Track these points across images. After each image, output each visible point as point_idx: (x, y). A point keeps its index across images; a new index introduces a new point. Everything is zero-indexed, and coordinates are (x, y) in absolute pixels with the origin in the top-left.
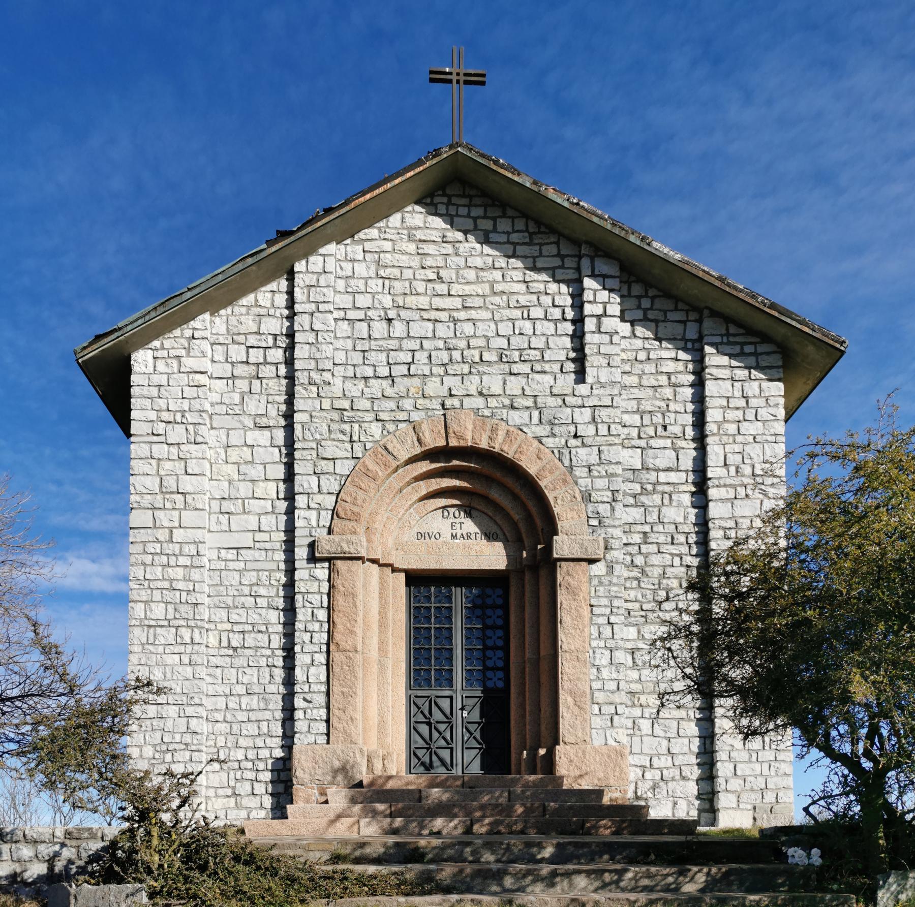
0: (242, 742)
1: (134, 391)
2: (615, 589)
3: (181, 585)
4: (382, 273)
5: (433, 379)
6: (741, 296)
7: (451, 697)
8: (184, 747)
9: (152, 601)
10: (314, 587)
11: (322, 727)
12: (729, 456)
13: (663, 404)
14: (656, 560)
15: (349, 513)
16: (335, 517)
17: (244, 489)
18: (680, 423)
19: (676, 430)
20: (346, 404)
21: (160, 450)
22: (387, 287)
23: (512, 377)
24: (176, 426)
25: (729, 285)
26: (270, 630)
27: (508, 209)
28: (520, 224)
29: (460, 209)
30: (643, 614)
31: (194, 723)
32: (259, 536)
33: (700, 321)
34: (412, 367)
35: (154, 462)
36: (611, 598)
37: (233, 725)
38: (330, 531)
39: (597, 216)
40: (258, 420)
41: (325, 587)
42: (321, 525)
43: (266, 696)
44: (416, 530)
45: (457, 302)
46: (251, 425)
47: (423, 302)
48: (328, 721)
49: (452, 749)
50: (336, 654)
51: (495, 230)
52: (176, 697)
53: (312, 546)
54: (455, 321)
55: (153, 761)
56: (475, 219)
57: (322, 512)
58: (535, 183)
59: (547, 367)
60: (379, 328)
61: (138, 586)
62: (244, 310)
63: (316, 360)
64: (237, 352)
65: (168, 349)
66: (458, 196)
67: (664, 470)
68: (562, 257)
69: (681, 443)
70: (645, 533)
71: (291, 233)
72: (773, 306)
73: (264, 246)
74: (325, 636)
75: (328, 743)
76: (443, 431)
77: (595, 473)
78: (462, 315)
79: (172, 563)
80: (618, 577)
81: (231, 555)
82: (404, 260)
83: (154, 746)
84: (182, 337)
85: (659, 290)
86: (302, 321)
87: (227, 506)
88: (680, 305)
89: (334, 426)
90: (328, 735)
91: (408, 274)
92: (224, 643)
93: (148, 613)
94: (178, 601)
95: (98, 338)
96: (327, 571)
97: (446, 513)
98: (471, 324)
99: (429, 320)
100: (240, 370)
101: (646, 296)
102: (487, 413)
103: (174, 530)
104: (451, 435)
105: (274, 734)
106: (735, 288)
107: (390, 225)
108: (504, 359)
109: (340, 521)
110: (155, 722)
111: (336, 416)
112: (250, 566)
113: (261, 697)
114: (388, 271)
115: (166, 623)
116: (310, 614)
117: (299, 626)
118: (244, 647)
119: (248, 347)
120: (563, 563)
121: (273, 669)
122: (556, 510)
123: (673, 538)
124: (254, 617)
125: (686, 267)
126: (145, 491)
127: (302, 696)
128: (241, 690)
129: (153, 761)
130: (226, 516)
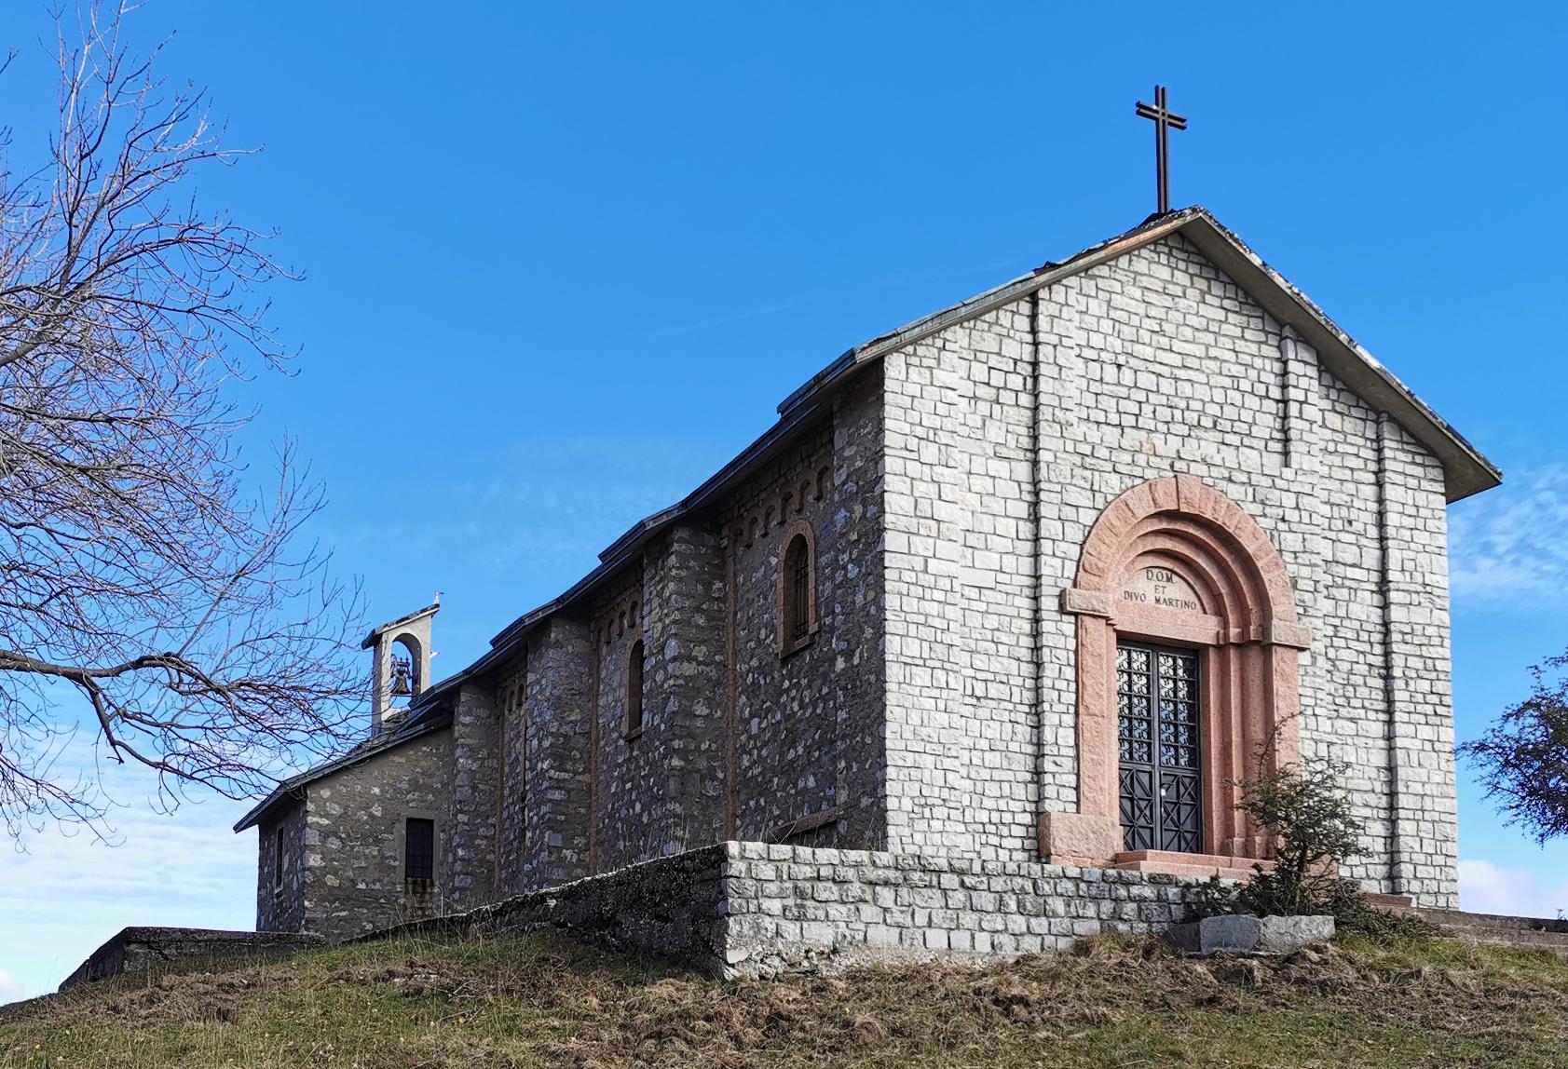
0: (988, 803)
1: (888, 397)
2: (1318, 680)
3: (937, 622)
4: (1113, 314)
5: (1157, 435)
6: (1425, 412)
7: (1150, 773)
8: (942, 803)
9: (907, 635)
10: (1060, 642)
11: (1072, 795)
12: (1405, 561)
13: (1348, 499)
14: (1344, 654)
15: (1094, 567)
16: (1081, 569)
17: (986, 524)
18: (1361, 520)
19: (1358, 526)
20: (1087, 450)
21: (913, 468)
22: (1117, 330)
23: (1225, 447)
24: (929, 444)
25: (1416, 401)
26: (1011, 682)
27: (1221, 273)
28: (1231, 289)
29: (1180, 262)
30: (1336, 708)
31: (950, 776)
32: (1001, 577)
33: (1378, 422)
34: (1140, 418)
35: (908, 480)
36: (1316, 689)
37: (977, 783)
38: (1075, 585)
39: (1314, 309)
40: (998, 449)
41: (1072, 644)
42: (1065, 576)
43: (1009, 754)
44: (1124, 589)
45: (1177, 360)
46: (992, 454)
47: (1148, 352)
48: (1077, 788)
49: (1152, 829)
50: (1086, 718)
51: (1209, 292)
52: (934, 746)
53: (1062, 596)
54: (1176, 379)
55: (912, 815)
56: (1192, 276)
57: (1066, 562)
58: (1264, 264)
59: (1255, 443)
60: (1111, 372)
61: (894, 618)
62: (986, 326)
63: (1060, 397)
64: (979, 372)
65: (920, 357)
66: (1177, 248)
67: (1351, 566)
68: (1267, 333)
69: (1363, 541)
70: (1335, 626)
71: (1059, 266)
72: (1449, 428)
73: (1032, 274)
74: (1074, 696)
75: (1078, 812)
76: (1174, 494)
77: (1299, 561)
78: (1182, 374)
79: (928, 596)
80: (1321, 669)
81: (974, 594)
82: (1133, 306)
83: (912, 798)
84: (933, 345)
85: (1345, 385)
86: (1045, 352)
87: (972, 539)
88: (1361, 404)
89: (1078, 471)
90: (1078, 803)
91: (1135, 321)
92: (969, 692)
93: (904, 649)
94: (933, 639)
95: (879, 340)
96: (1073, 627)
97: (1150, 574)
98: (1189, 384)
99: (1154, 373)
100: (983, 391)
101: (1333, 387)
102: (1210, 481)
103: (929, 560)
104: (1182, 501)
105: (1017, 797)
106: (1421, 405)
107: (1120, 265)
108: (1218, 428)
109: (1085, 574)
110: (913, 772)
111: (1078, 460)
112: (992, 608)
113: (1003, 754)
114: (1119, 313)
115: (921, 662)
116: (1057, 671)
117: (1047, 682)
118: (986, 698)
119: (990, 368)
120: (1279, 649)
121: (1016, 725)
122: (1271, 594)
123: (1358, 635)
124: (996, 666)
125: (1382, 374)
126: (901, 512)
127: (1052, 758)
128: (984, 744)
129: (912, 815)
130: (971, 550)
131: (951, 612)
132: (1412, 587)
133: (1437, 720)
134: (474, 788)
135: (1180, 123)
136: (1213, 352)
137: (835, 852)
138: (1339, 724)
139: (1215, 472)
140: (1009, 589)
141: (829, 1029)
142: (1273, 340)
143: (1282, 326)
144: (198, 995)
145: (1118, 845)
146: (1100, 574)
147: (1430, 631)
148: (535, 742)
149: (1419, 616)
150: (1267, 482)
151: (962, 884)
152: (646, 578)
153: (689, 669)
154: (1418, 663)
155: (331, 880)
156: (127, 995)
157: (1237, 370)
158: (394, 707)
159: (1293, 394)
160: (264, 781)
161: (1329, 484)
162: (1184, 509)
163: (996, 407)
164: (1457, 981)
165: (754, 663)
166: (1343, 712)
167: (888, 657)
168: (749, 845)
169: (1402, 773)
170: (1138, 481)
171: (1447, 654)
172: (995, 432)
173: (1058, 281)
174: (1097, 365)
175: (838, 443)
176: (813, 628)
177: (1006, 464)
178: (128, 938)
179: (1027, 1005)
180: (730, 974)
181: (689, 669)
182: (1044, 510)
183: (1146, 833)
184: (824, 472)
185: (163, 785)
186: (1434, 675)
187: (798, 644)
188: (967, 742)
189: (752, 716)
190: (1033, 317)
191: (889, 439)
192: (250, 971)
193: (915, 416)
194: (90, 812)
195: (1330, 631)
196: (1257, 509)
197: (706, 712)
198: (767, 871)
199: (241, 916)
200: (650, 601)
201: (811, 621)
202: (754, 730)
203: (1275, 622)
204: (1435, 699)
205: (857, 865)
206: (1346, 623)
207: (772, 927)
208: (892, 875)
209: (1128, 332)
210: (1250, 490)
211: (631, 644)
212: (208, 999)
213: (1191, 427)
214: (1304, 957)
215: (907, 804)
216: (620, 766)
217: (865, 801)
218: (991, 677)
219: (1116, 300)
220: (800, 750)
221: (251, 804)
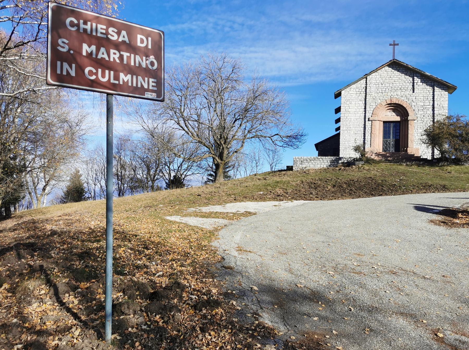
11: (370, 145)
33: (434, 82)
41: (371, 125)
47: (388, 81)
53: (369, 119)
60: (380, 85)
64: (357, 90)
69: (430, 101)
78: (394, 83)
81: (356, 120)
82: (385, 75)
100: (358, 93)
136: (400, 78)
139: (399, 96)
159: (415, 81)
172: (360, 98)
183: (389, 149)
190: (366, 81)
193: (346, 98)
198: (298, 160)
208: (313, 159)
209: (384, 79)
215: (343, 148)
219: (382, 75)
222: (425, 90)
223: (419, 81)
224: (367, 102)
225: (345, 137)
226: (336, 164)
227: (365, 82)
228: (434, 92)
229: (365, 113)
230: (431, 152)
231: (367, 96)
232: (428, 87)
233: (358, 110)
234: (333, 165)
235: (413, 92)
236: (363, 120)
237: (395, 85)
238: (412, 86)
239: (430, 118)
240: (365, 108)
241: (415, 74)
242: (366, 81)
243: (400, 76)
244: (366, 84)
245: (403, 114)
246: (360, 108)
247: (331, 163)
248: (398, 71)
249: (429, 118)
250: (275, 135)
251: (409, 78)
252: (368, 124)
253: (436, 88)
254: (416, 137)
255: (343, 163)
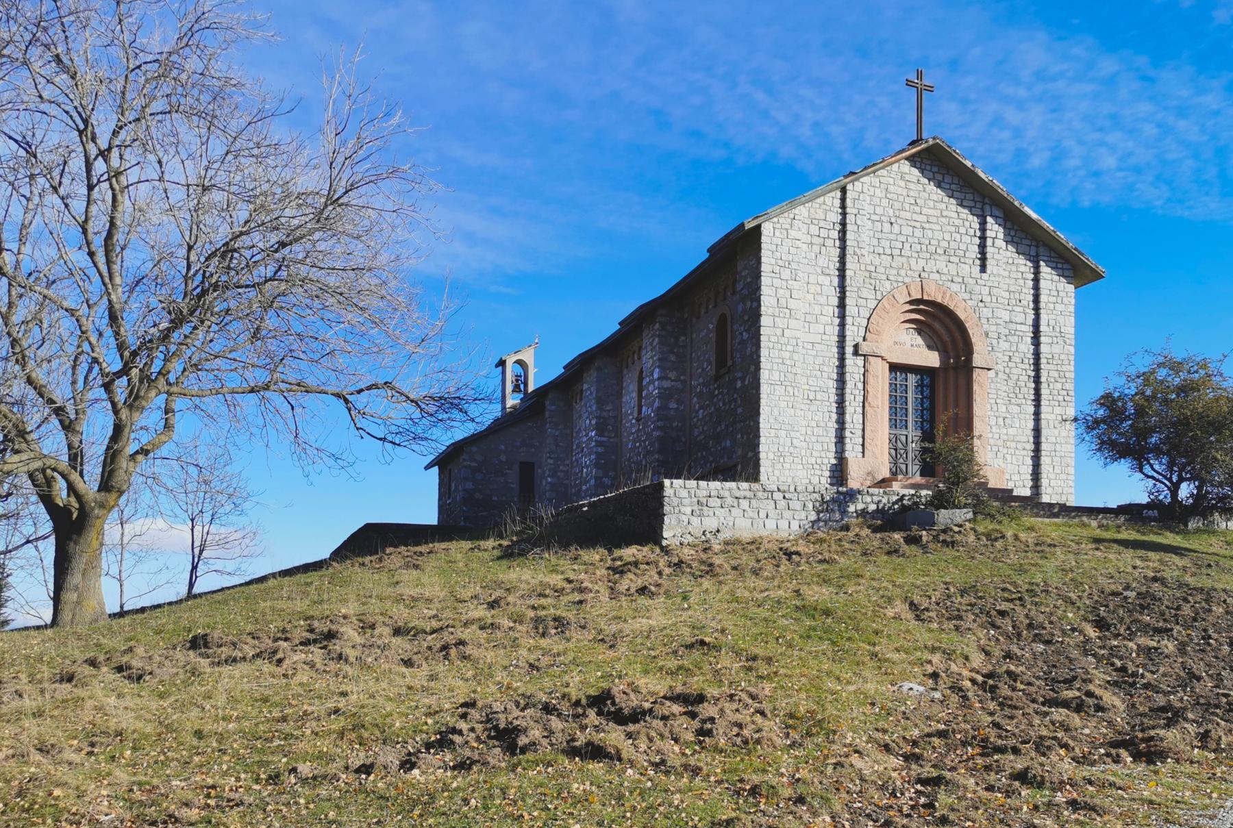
11: (860, 448)
20: (873, 269)
21: (777, 282)
32: (824, 337)
33: (1037, 247)
47: (908, 215)
51: (943, 181)
53: (856, 347)
59: (967, 261)
60: (887, 226)
64: (814, 230)
68: (975, 202)
69: (1028, 310)
78: (927, 226)
82: (900, 191)
89: (867, 280)
90: (863, 452)
100: (816, 240)
117: (848, 391)
122: (973, 340)
131: (796, 357)
132: (1053, 334)
133: (1065, 404)
134: (557, 445)
135: (930, 89)
136: (945, 213)
137: (719, 483)
138: (1010, 407)
139: (944, 278)
140: (828, 343)
141: (703, 567)
142: (979, 205)
143: (984, 197)
144: (404, 557)
145: (885, 473)
146: (878, 333)
147: (1063, 357)
148: (588, 421)
149: (1056, 349)
150: (972, 281)
151: (784, 497)
152: (644, 335)
153: (666, 384)
154: (1056, 374)
155: (478, 496)
156: (369, 558)
157: (957, 222)
158: (513, 401)
159: (989, 233)
160: (439, 445)
161: (1008, 281)
162: (925, 298)
163: (823, 248)
164: (1023, 539)
165: (701, 380)
166: (1013, 401)
167: (762, 381)
168: (675, 481)
169: (1044, 432)
170: (900, 284)
171: (1072, 369)
172: (822, 261)
173: (857, 179)
174: (879, 224)
175: (739, 269)
176: (730, 363)
177: (828, 278)
178: (368, 528)
179: (800, 555)
180: (664, 543)
181: (666, 384)
182: (848, 301)
183: (903, 467)
184: (735, 282)
185: (384, 448)
186: (1064, 380)
187: (723, 371)
188: (804, 423)
189: (700, 408)
190: (843, 200)
191: (764, 268)
192: (431, 545)
194: (346, 464)
195: (1007, 359)
196: (966, 296)
197: (675, 406)
198: (684, 493)
199: (430, 517)
200: (646, 347)
201: (729, 358)
202: (701, 416)
203: (975, 355)
204: (1065, 393)
205: (730, 490)
206: (1016, 354)
207: (686, 521)
210: (963, 286)
211: (639, 369)
212: (409, 559)
213: (931, 254)
214: (951, 530)
215: (771, 456)
216: (633, 434)
217: (750, 454)
218: (818, 389)
219: (891, 188)
220: (723, 426)
221: (431, 458)
222: (1014, 268)
223: (1001, 235)
224: (848, 281)
225: (776, 412)
226: (837, 516)
227: (837, 203)
228: (1036, 280)
229: (842, 325)
230: (1031, 483)
231: (849, 258)
232: (1021, 260)
233: (817, 310)
234: (826, 522)
235: (983, 268)
236: (835, 350)
237: (929, 233)
238: (976, 249)
239: (1027, 367)
240: (842, 305)
241: (987, 208)
242: (843, 200)
243: (944, 206)
244: (844, 214)
245: (950, 346)
246: (823, 300)
247: (818, 512)
248: (939, 186)
249: (1023, 366)
250: (369, 388)
251: (971, 217)
252: (854, 365)
253: (1045, 269)
254: (994, 429)
255: (863, 513)
